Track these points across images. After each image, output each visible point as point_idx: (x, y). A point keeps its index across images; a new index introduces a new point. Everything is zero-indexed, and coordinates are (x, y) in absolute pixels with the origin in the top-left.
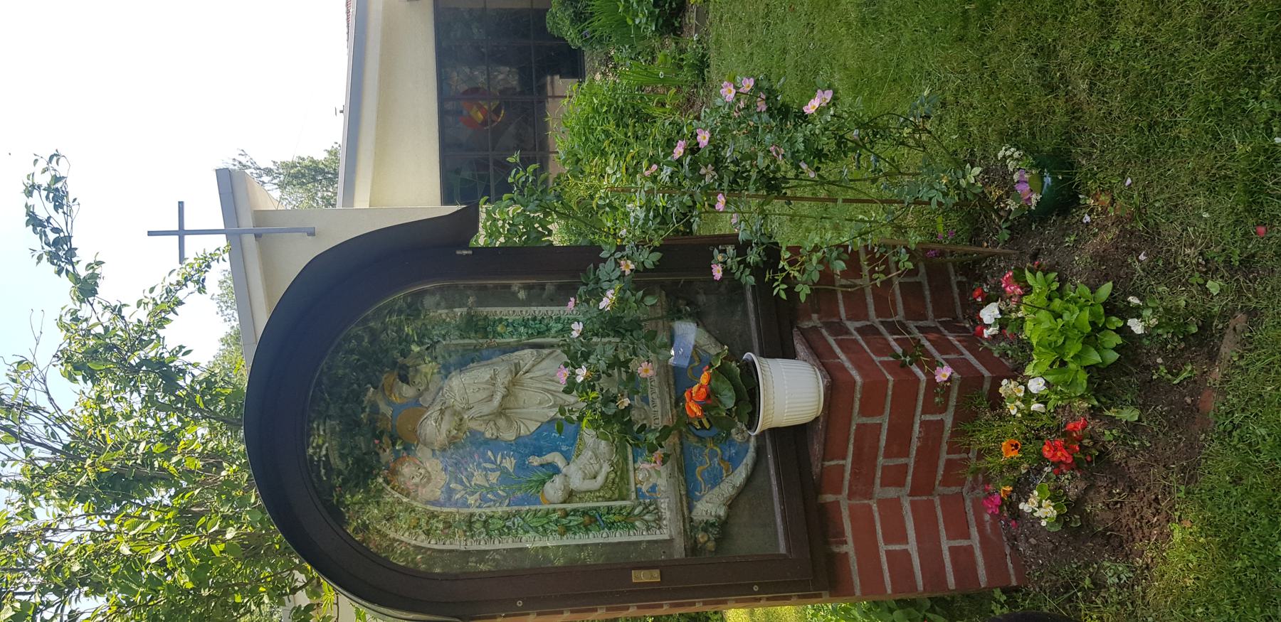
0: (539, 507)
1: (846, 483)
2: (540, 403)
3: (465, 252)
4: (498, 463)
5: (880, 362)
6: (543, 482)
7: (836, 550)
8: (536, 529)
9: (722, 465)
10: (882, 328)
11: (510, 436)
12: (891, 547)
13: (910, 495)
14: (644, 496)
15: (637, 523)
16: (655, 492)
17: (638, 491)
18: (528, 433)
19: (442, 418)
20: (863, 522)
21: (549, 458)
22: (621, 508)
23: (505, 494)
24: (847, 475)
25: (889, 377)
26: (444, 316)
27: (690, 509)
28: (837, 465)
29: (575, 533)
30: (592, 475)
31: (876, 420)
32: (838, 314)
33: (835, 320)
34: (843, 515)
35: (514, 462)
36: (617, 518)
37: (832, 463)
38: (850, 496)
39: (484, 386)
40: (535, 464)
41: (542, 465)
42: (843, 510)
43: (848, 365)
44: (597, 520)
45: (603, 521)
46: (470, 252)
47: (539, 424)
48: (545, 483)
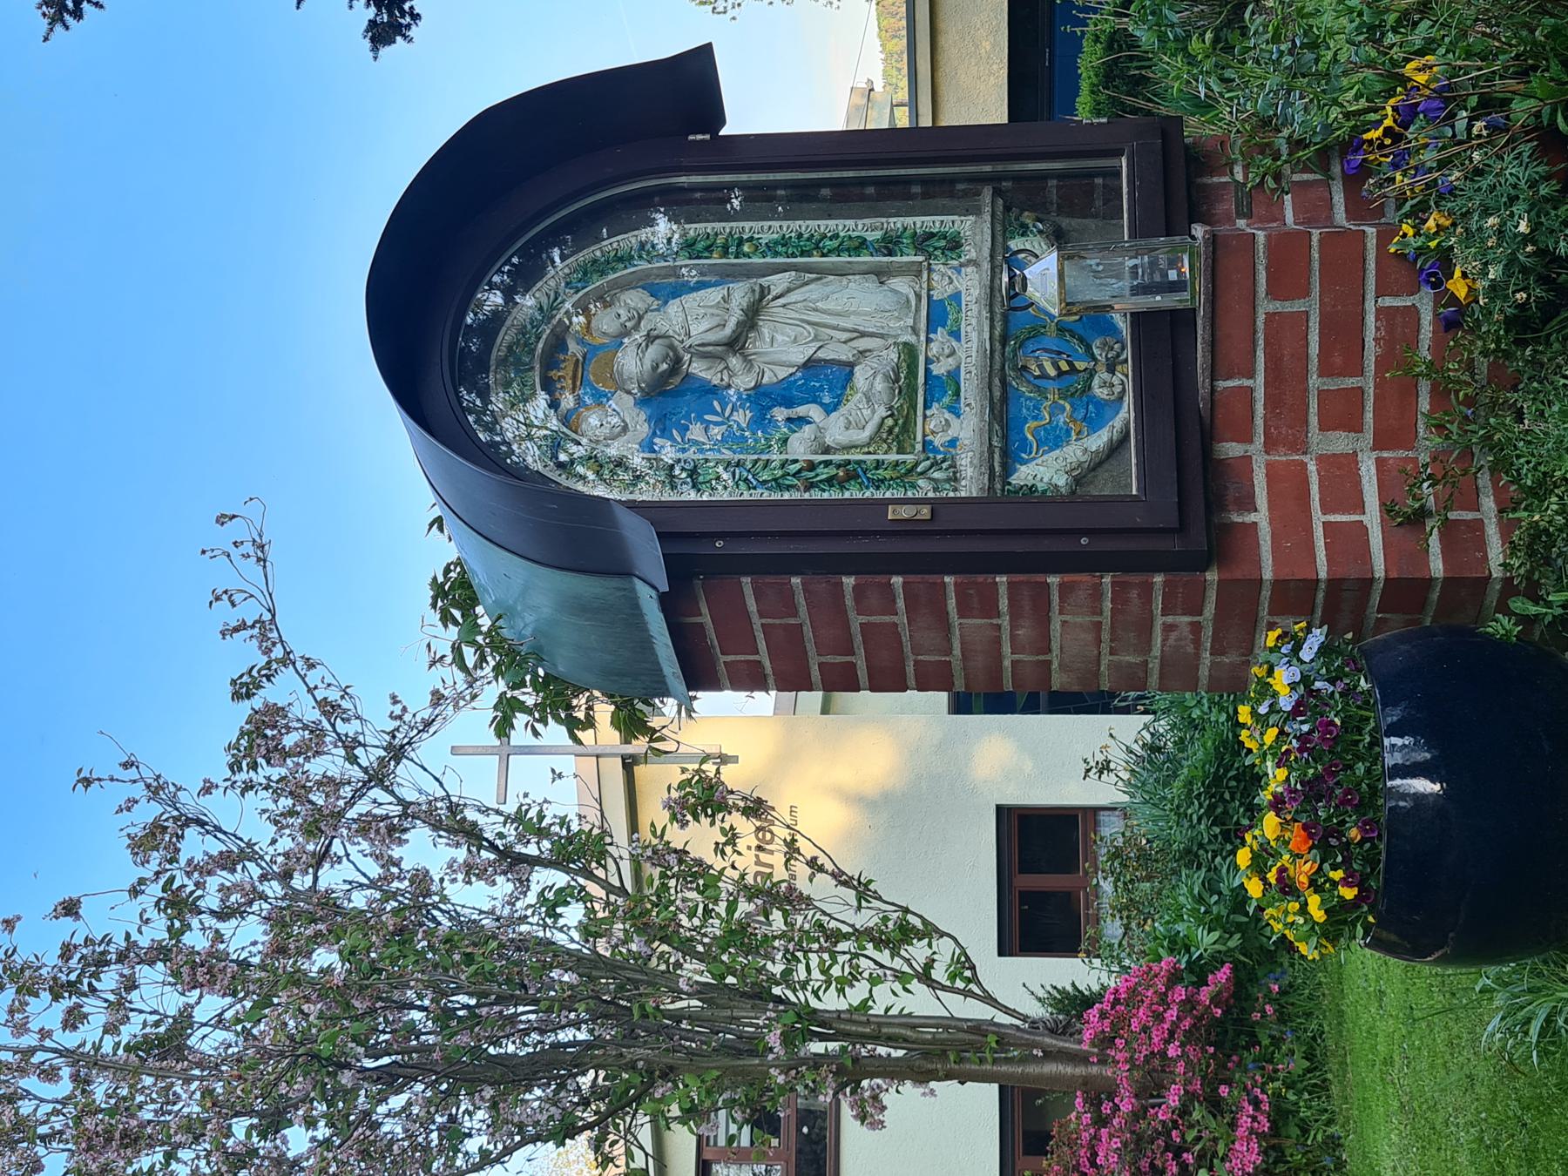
1: (1259, 422)
4: (727, 415)
13: (1373, 449)
16: (955, 447)
18: (775, 380)
20: (1289, 488)
21: (801, 410)
22: (897, 464)
27: (1008, 470)
28: (1240, 387)
31: (1297, 306)
35: (749, 415)
36: (888, 474)
37: (1230, 383)
38: (1269, 446)
44: (859, 476)
45: (868, 478)
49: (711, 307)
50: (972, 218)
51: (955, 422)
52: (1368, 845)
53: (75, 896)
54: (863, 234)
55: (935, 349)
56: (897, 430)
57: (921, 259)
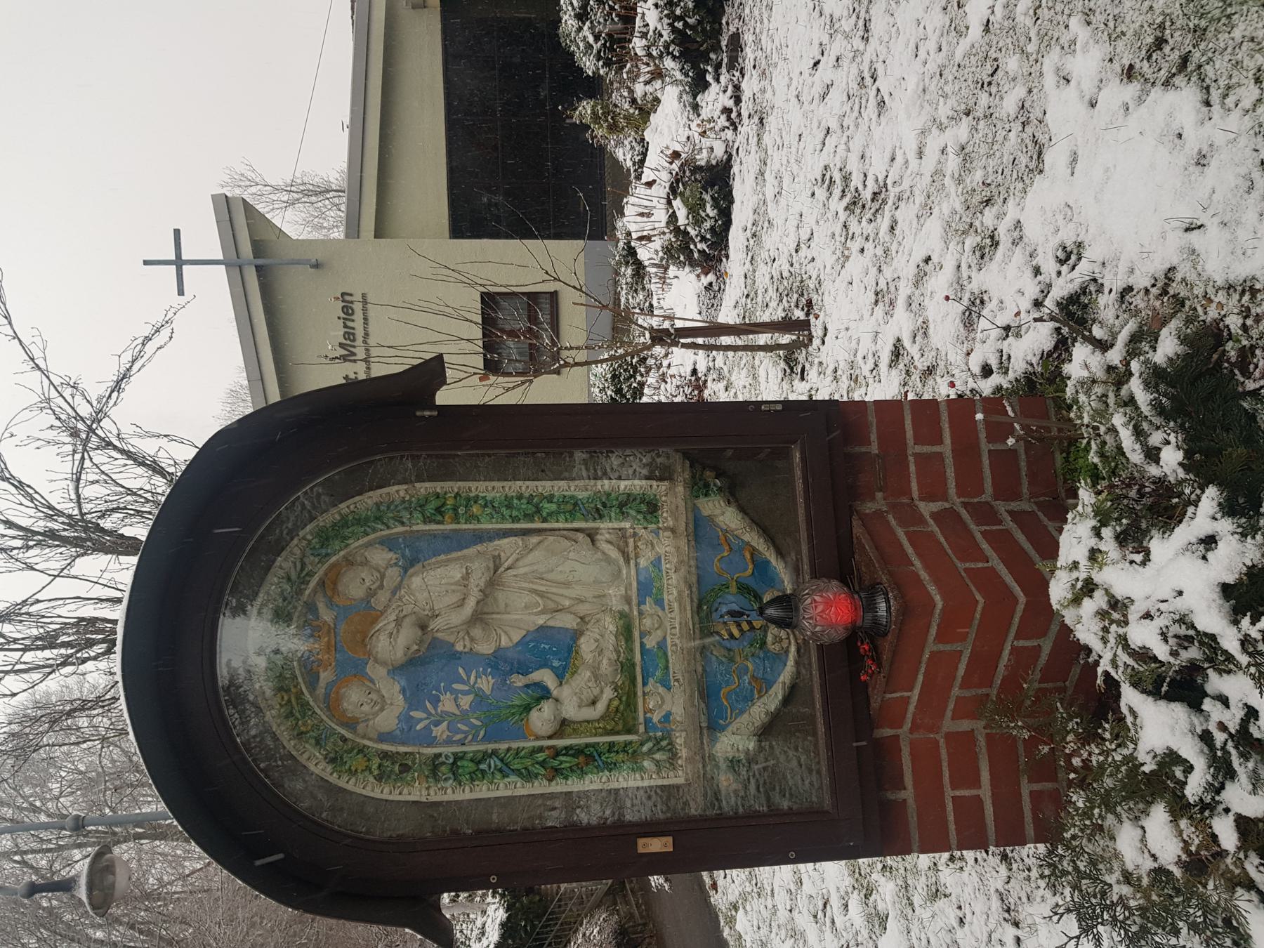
0: (521, 744)
1: (909, 716)
2: (526, 607)
3: (427, 413)
5: (966, 570)
6: (527, 708)
7: (891, 796)
8: (518, 772)
9: (754, 684)
10: (964, 513)
11: (485, 648)
12: (958, 793)
14: (655, 728)
15: (646, 763)
16: (669, 722)
17: (647, 721)
19: (398, 632)
23: (480, 724)
24: (912, 708)
25: (978, 597)
26: (402, 493)
29: (566, 778)
30: (590, 701)
31: (957, 647)
32: (908, 492)
33: (905, 500)
34: (903, 752)
35: (492, 681)
39: (453, 587)
40: (520, 684)
41: (527, 686)
42: (903, 747)
43: (924, 575)
46: (435, 413)
47: (524, 633)
48: (530, 710)
49: (452, 584)
50: (666, 483)
51: (668, 697)
54: (575, 493)
55: (647, 622)
56: (621, 707)
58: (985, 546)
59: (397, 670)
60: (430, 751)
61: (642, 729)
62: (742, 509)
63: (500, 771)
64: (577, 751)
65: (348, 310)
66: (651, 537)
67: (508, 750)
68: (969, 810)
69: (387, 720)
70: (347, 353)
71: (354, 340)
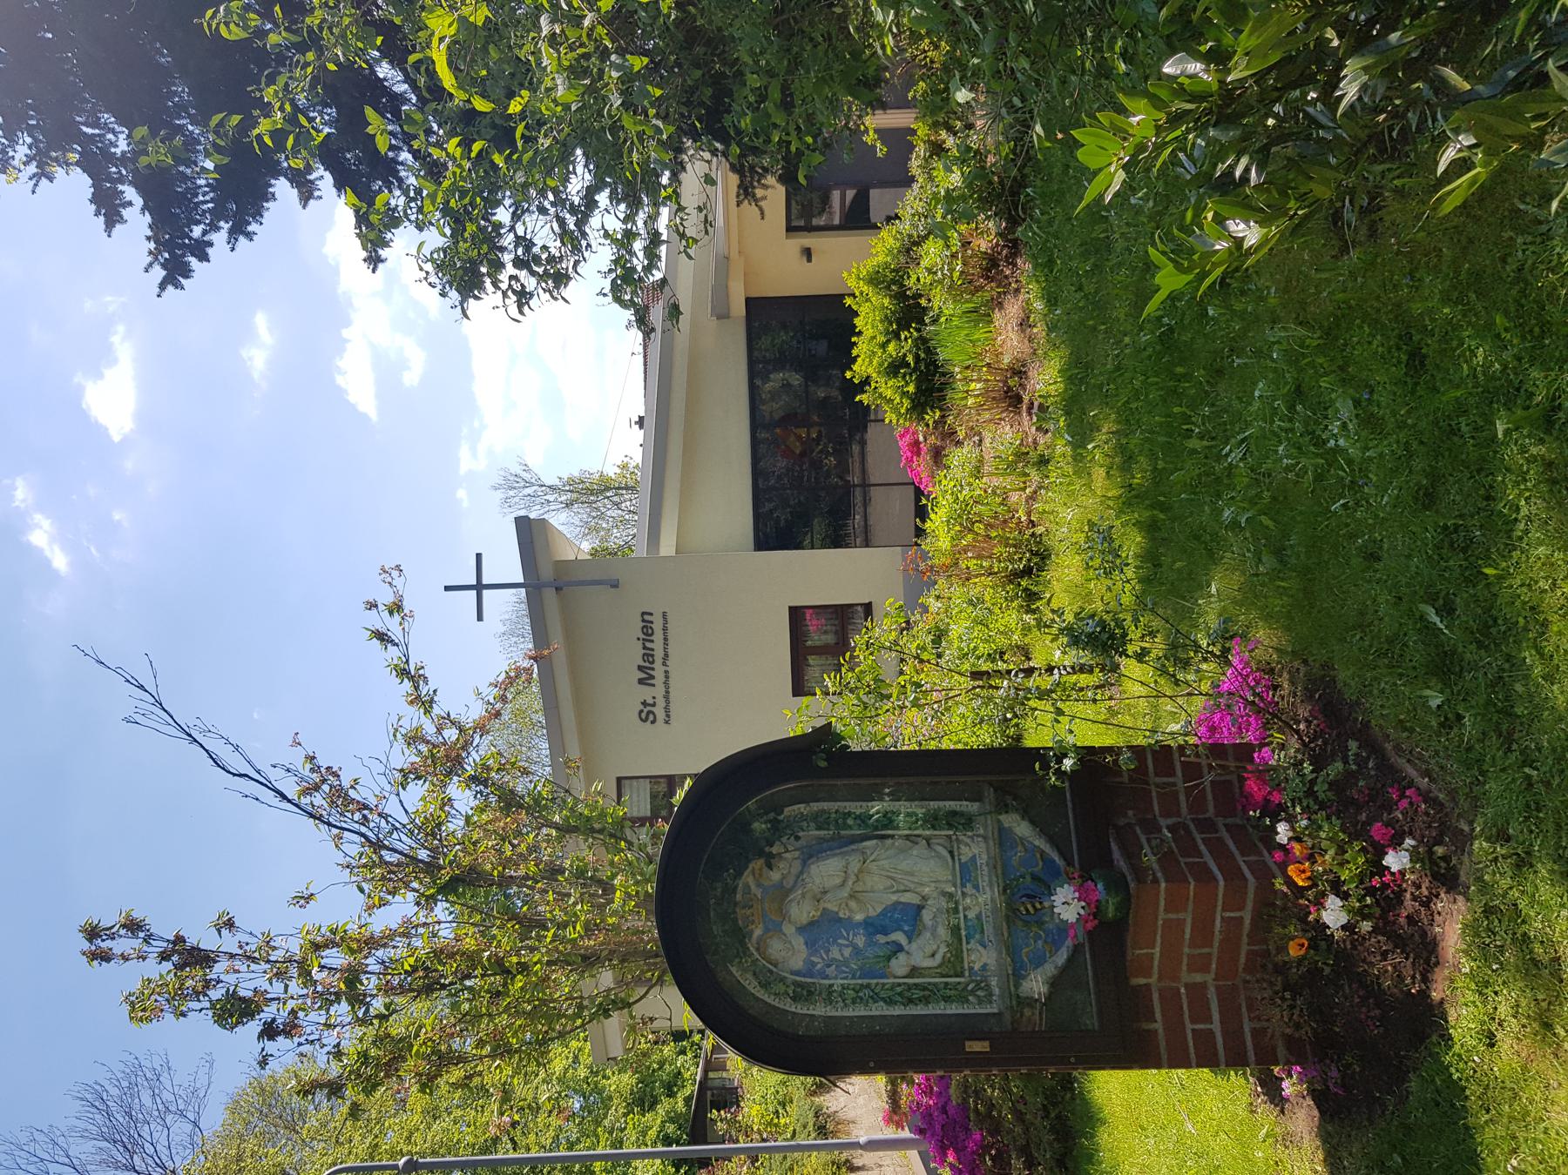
0: (885, 981)
6: (889, 959)
8: (883, 999)
10: (1192, 826)
17: (971, 969)
25: (1191, 880)
27: (1017, 986)
31: (1181, 916)
52: (1179, 370)
53: (118, 229)
57: (951, 833)
58: (1202, 848)
59: (801, 930)
60: (827, 982)
61: (967, 974)
62: (1033, 822)
63: (872, 997)
64: (923, 988)
65: (647, 631)
66: (968, 841)
67: (877, 984)
68: (1205, 1038)
69: (797, 963)
70: (645, 676)
71: (653, 662)
